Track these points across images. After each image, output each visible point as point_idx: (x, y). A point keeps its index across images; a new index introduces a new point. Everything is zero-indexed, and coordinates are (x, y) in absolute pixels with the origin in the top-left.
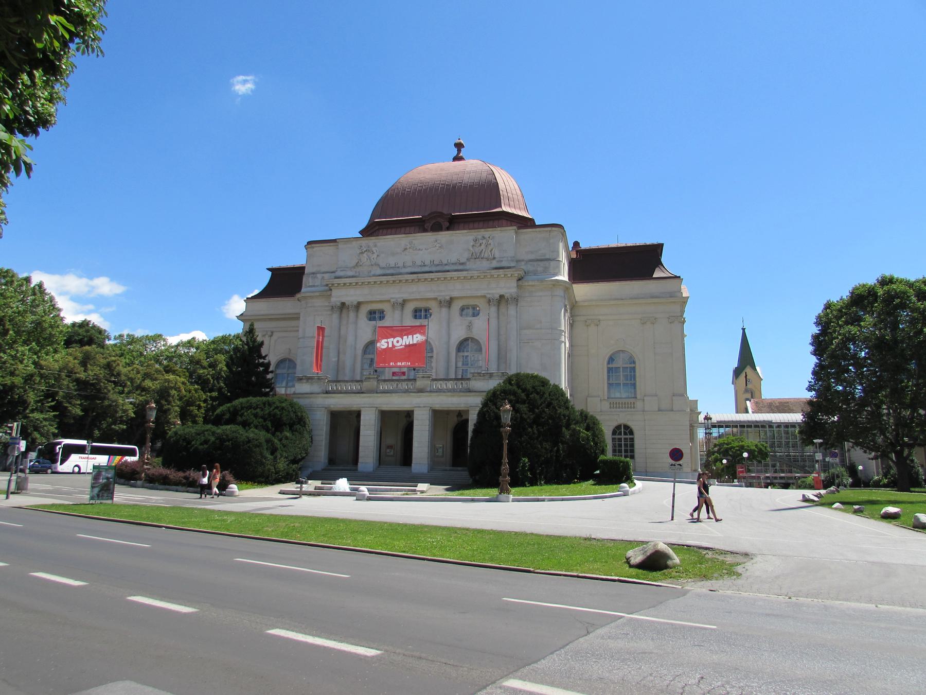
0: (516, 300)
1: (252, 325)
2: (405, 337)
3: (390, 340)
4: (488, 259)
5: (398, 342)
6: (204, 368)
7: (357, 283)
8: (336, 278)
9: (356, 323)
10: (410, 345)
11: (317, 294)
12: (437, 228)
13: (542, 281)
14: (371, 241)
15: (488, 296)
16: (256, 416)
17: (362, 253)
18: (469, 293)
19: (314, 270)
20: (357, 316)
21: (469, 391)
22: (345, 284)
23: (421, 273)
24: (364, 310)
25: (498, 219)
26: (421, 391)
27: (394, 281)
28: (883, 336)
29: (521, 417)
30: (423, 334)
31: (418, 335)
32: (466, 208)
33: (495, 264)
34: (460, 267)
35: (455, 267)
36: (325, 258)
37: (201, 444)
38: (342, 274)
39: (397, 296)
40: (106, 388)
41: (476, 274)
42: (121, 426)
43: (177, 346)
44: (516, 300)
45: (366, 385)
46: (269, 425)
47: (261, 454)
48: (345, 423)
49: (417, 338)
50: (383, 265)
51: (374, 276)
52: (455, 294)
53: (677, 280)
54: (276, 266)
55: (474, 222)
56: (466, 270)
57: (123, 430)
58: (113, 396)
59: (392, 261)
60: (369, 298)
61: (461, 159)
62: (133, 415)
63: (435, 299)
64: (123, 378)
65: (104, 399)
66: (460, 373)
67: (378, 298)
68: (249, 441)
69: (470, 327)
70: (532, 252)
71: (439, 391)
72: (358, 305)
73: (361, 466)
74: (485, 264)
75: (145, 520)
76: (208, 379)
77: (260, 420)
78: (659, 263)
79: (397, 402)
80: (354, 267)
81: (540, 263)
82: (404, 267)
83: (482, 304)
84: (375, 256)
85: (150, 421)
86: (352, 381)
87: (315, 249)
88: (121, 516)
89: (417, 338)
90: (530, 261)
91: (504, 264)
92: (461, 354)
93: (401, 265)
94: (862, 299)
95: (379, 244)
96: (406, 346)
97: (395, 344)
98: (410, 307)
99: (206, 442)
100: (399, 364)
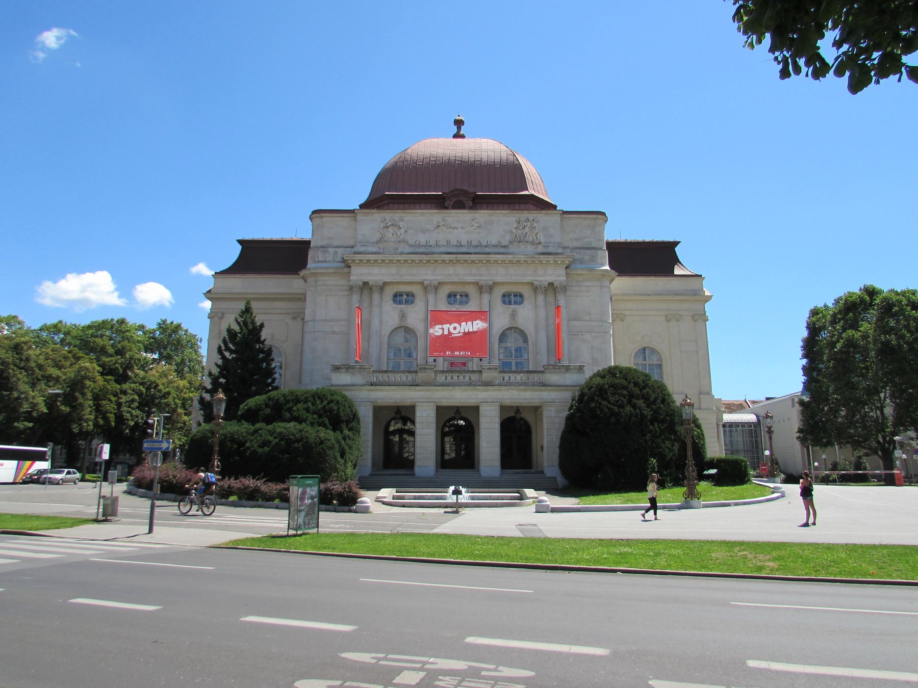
0: (564, 289)
1: (248, 303)
2: (463, 324)
3: (446, 326)
4: (533, 243)
5: (455, 328)
6: (111, 356)
7: (383, 261)
8: (355, 253)
9: (380, 306)
10: (469, 333)
11: (331, 271)
12: (459, 206)
13: (592, 270)
14: (378, 217)
15: (481, 283)
16: (307, 410)
17: (387, 227)
18: (514, 279)
19: (324, 243)
20: (381, 299)
21: (544, 385)
22: (368, 261)
23: (459, 253)
24: (389, 292)
25: (525, 203)
26: (488, 384)
27: (428, 261)
28: (889, 342)
29: (642, 414)
30: (485, 320)
31: (478, 322)
32: (493, 187)
33: (540, 249)
34: (502, 249)
35: (497, 250)
36: (338, 229)
37: (260, 446)
38: (362, 249)
39: (430, 278)
40: (14, 375)
41: (523, 258)
42: (26, 423)
43: (41, 329)
44: (564, 289)
45: (421, 376)
46: (327, 422)
47: (335, 458)
48: (397, 421)
49: (478, 325)
50: (411, 242)
51: (401, 253)
52: (499, 279)
53: (699, 278)
54: (248, 237)
55: (520, 203)
56: (510, 254)
57: (29, 428)
58: (24, 387)
59: (422, 239)
60: (397, 279)
61: (463, 137)
62: (45, 411)
63: (476, 283)
64: (33, 364)
65: (11, 390)
66: (391, 365)
67: (408, 279)
68: (321, 443)
69: (513, 315)
70: (577, 240)
71: (509, 384)
72: (382, 287)
73: (417, 470)
74: (530, 249)
75: (444, 557)
76: (117, 368)
77: (315, 416)
78: (676, 261)
79: (459, 396)
80: (377, 242)
81: (587, 251)
82: (438, 246)
83: (526, 292)
84: (403, 231)
85: (219, 417)
86: (410, 372)
87: (325, 219)
88: (433, 555)
89: (478, 325)
90: (576, 248)
91: (550, 250)
92: (504, 345)
93: (433, 243)
94: (852, 308)
95: (406, 219)
96: (464, 333)
97: (452, 330)
98: (445, 291)
99: (264, 444)
100: (457, 353)
